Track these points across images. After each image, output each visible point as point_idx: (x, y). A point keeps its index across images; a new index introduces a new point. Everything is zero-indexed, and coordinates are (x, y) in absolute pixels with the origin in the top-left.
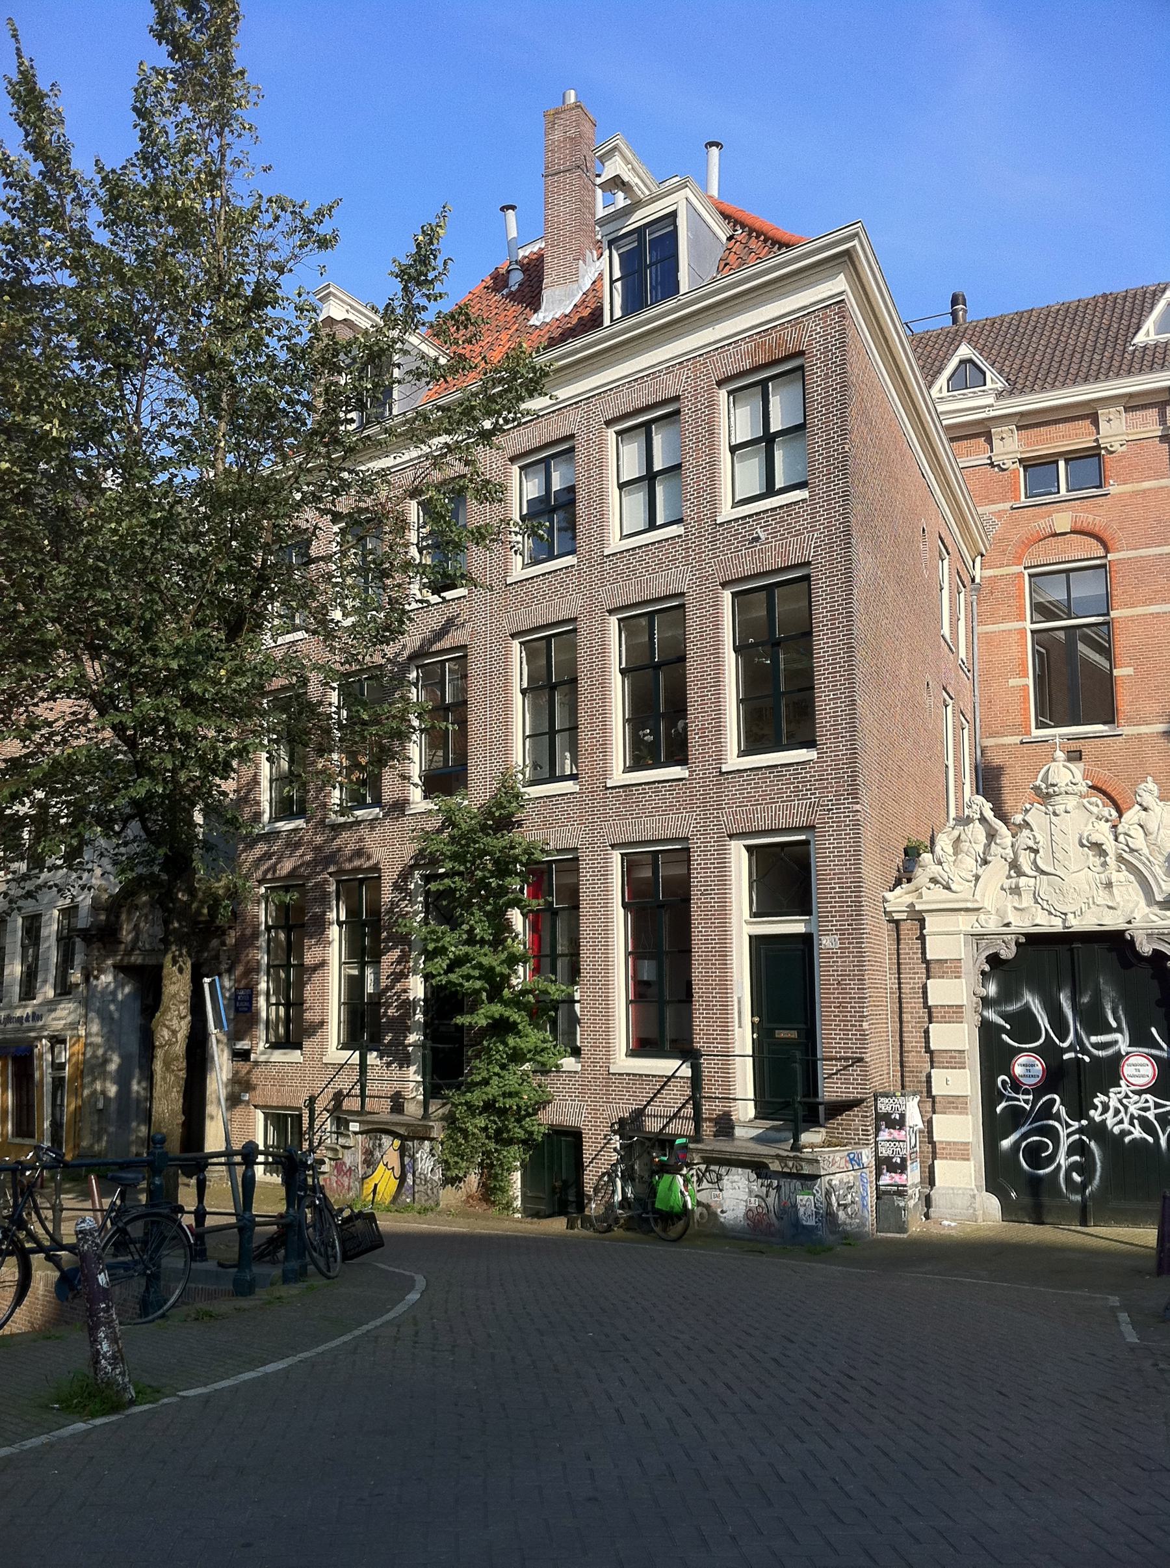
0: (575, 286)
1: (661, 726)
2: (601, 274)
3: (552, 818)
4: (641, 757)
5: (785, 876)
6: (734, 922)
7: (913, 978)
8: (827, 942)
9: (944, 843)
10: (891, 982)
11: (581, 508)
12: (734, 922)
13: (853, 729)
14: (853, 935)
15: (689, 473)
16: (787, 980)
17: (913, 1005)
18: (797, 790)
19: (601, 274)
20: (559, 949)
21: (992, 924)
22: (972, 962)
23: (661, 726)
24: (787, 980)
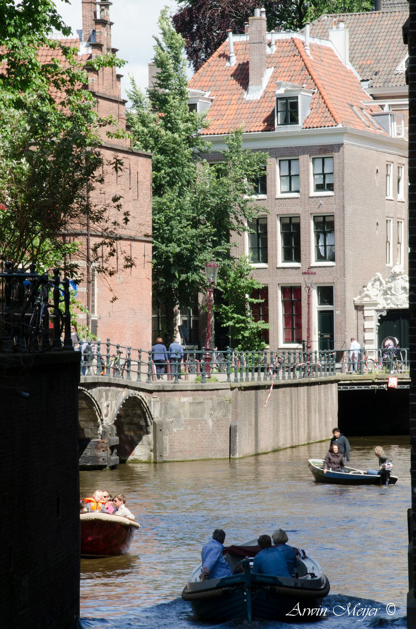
0: (260, 87)
1: (293, 251)
2: (274, 109)
3: (259, 274)
4: (288, 257)
5: (326, 294)
6: (314, 306)
7: (361, 321)
8: (337, 313)
9: (369, 285)
10: (355, 322)
11: (268, 181)
12: (314, 306)
13: (344, 259)
14: (344, 311)
15: (301, 176)
16: (327, 321)
17: (361, 328)
18: (330, 273)
19: (274, 109)
20: (261, 311)
21: (380, 307)
22: (376, 316)
23: (293, 251)
24: (327, 321)
